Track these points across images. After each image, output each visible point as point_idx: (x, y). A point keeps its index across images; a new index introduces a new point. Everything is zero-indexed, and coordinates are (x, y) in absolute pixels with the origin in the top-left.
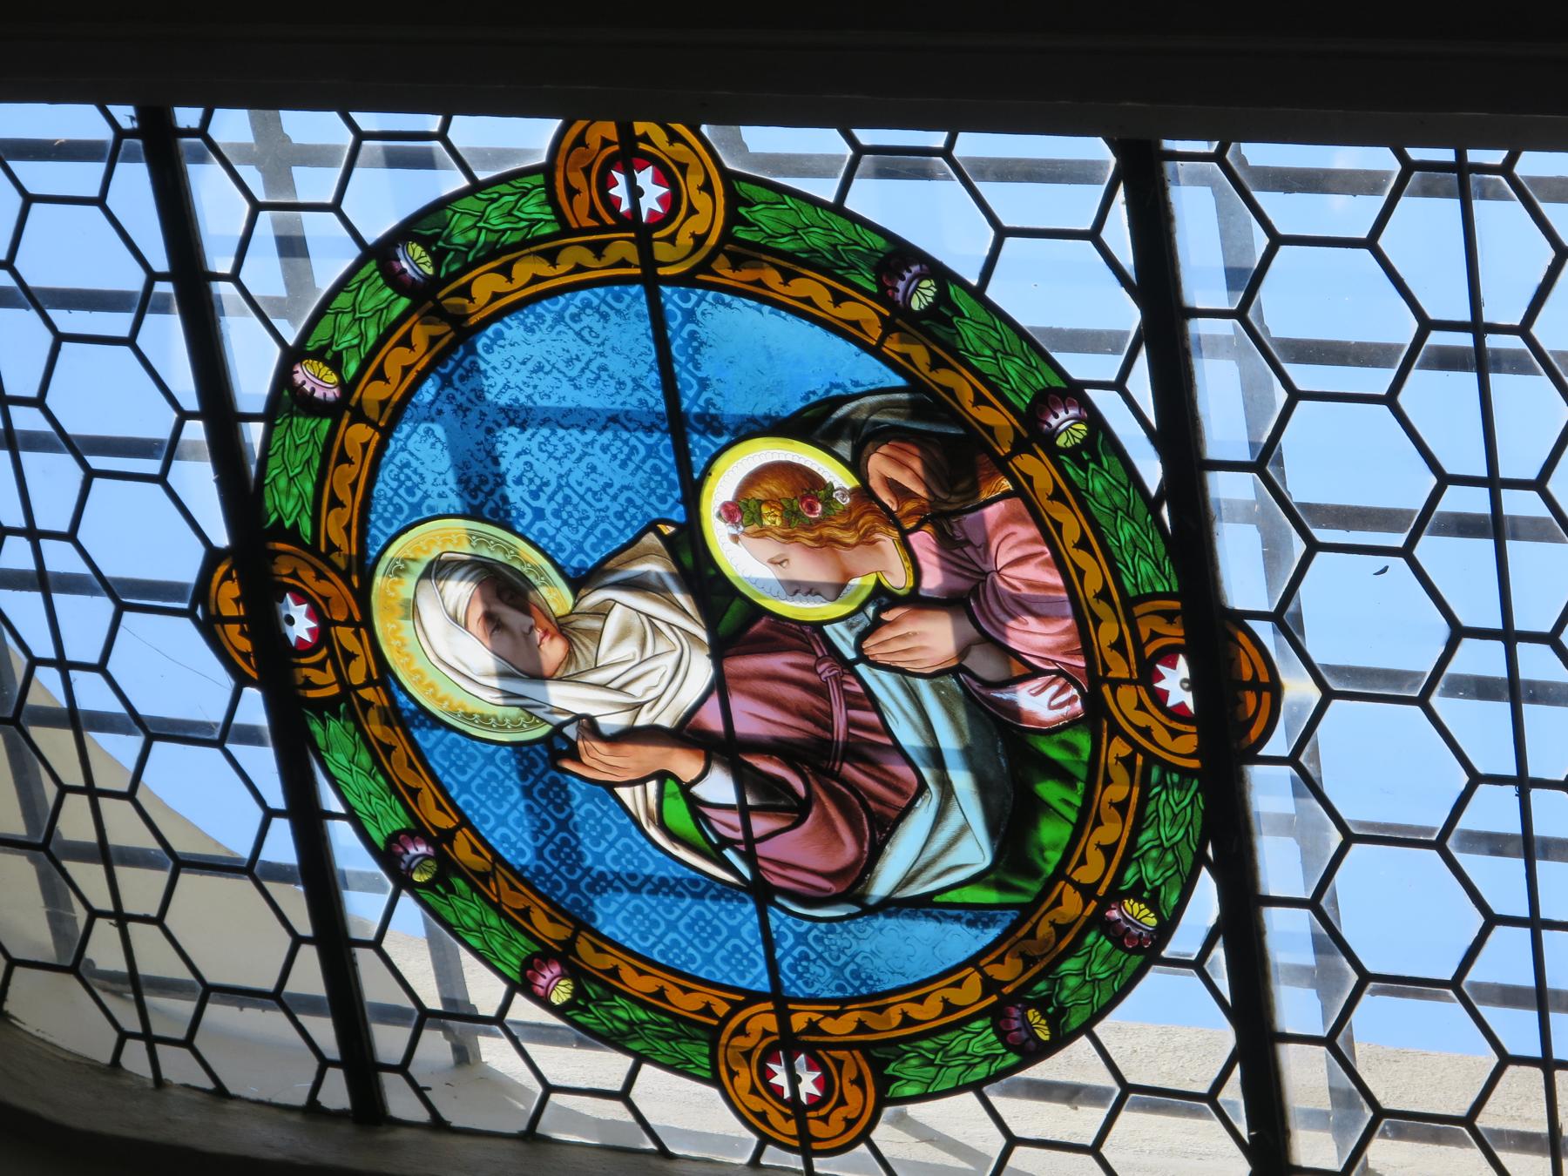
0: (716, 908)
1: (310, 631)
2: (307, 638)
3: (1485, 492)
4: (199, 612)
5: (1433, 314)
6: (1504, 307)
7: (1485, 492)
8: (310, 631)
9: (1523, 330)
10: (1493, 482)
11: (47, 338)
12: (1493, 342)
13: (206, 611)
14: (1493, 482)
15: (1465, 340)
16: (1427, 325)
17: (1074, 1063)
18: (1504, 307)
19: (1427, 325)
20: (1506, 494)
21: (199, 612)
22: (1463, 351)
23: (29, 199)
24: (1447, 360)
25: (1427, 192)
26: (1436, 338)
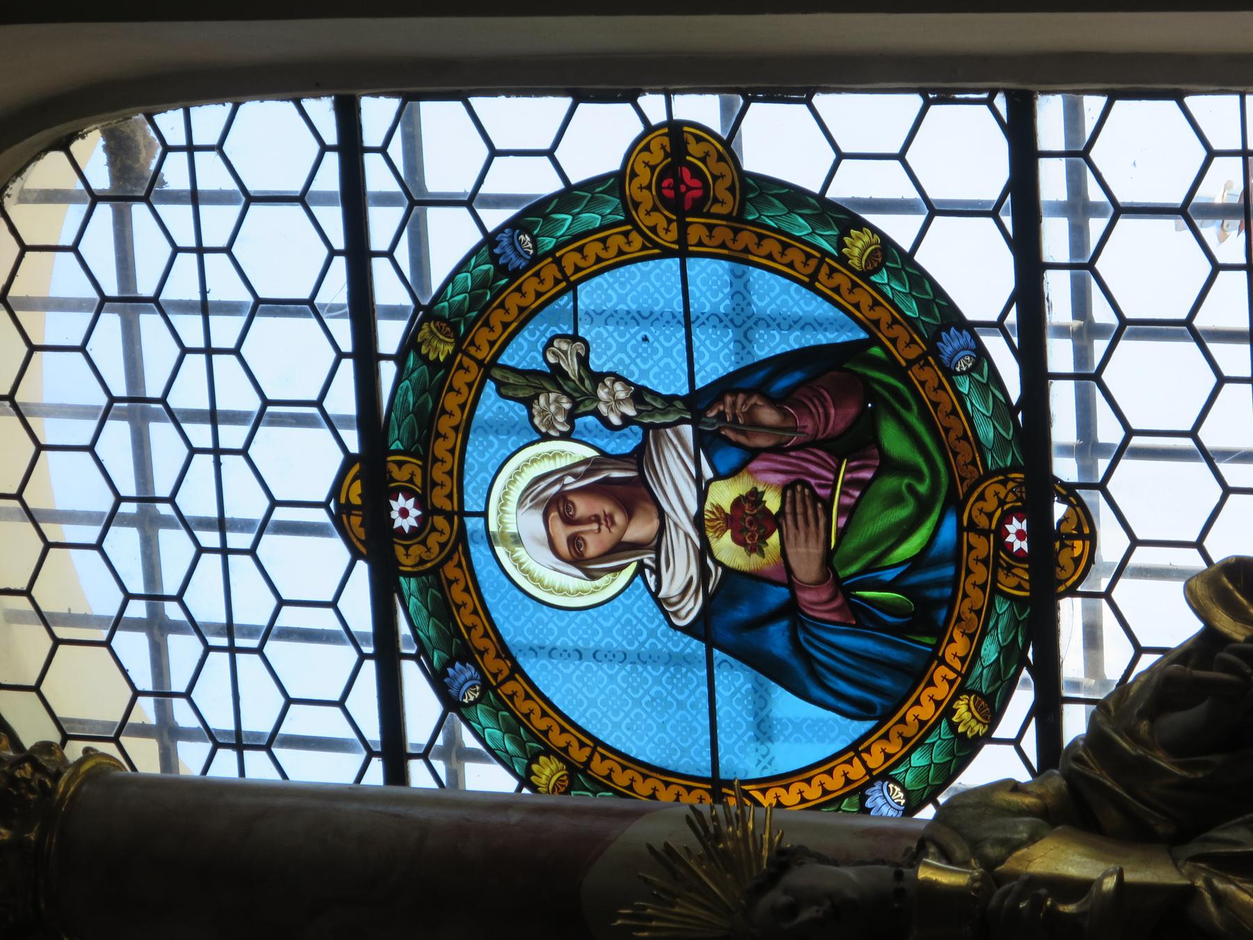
0: (796, 309)
1: (396, 499)
2: (401, 496)
3: (230, 545)
4: (332, 505)
5: (256, 657)
6: (219, 661)
7: (230, 545)
8: (396, 499)
9: (208, 649)
10: (225, 551)
11: (192, 550)
12: (224, 642)
13: (337, 504)
14: (225, 551)
15: (239, 642)
16: (259, 651)
17: (494, 218)
18: (219, 661)
19: (259, 651)
20: (217, 545)
21: (332, 505)
22: (244, 636)
23: (333, 605)
24: (250, 631)
25: (259, 735)
26: (254, 643)
